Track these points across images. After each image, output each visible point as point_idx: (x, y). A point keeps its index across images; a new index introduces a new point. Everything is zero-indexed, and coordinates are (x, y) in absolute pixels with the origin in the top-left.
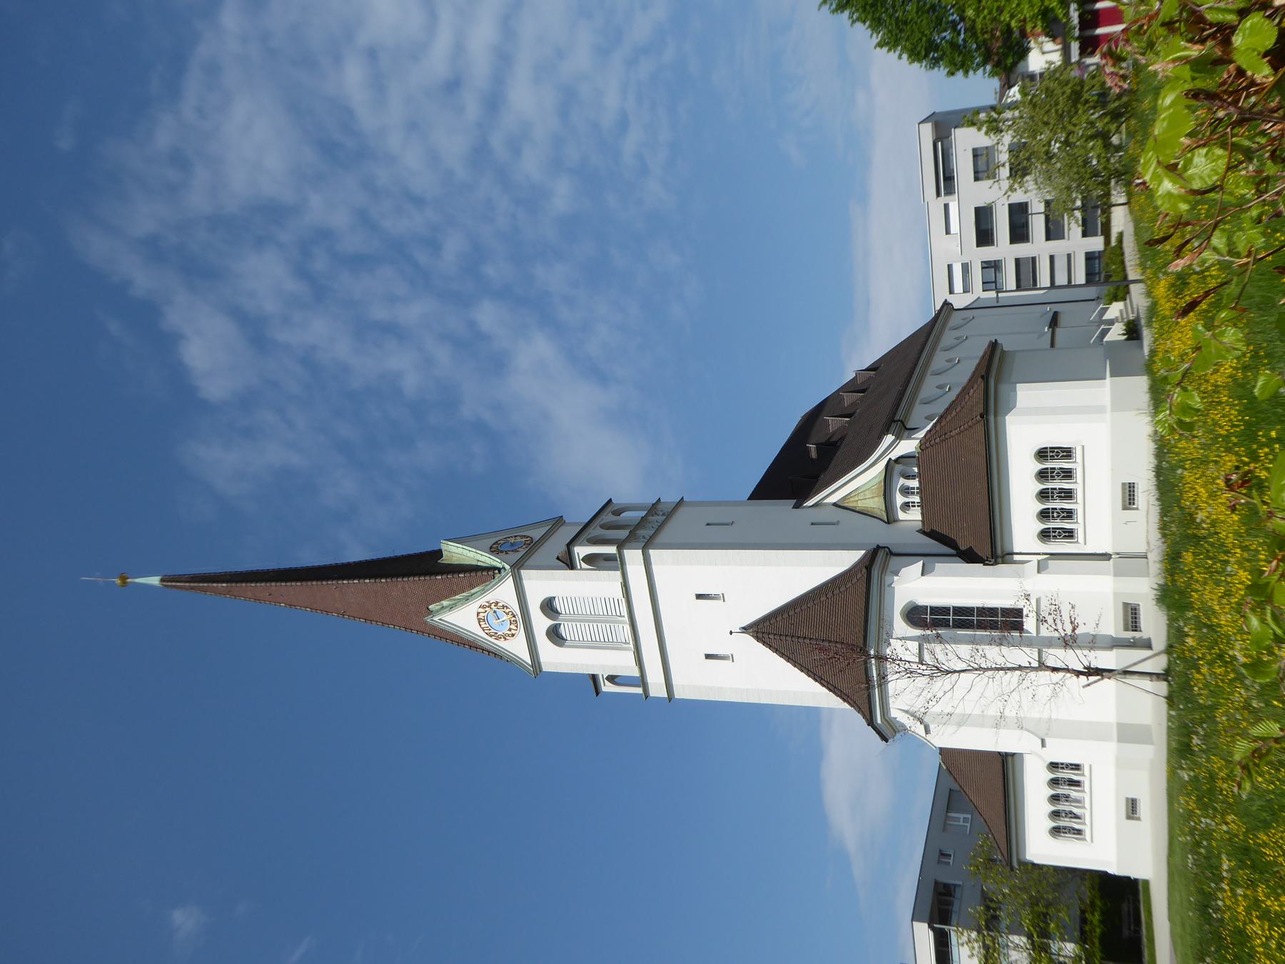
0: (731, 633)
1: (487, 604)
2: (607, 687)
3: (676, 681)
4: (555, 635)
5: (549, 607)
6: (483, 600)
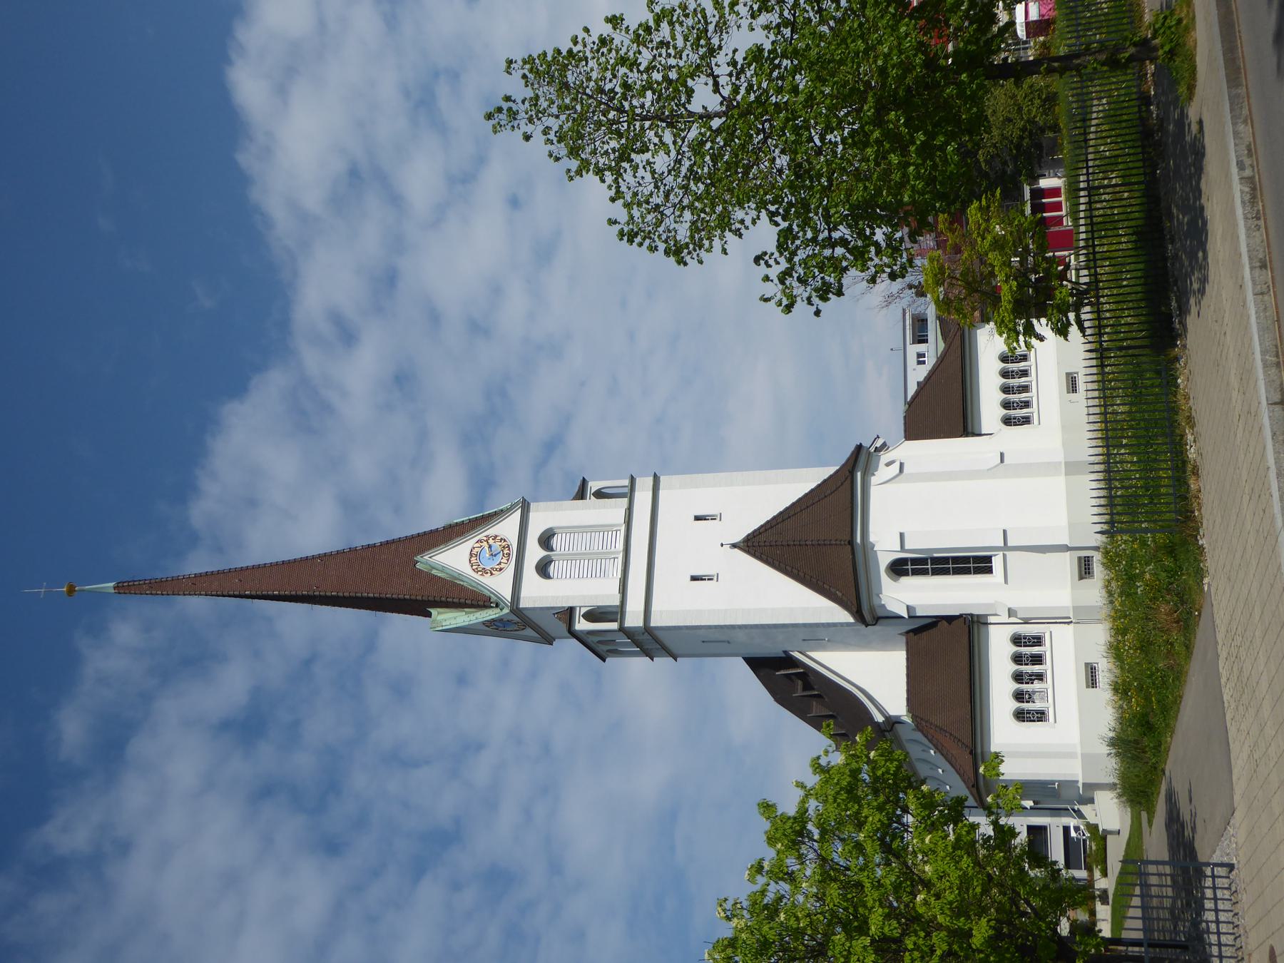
0: (722, 545)
1: (485, 539)
2: (582, 625)
3: (655, 607)
4: (543, 569)
5: (546, 540)
6: (477, 576)
